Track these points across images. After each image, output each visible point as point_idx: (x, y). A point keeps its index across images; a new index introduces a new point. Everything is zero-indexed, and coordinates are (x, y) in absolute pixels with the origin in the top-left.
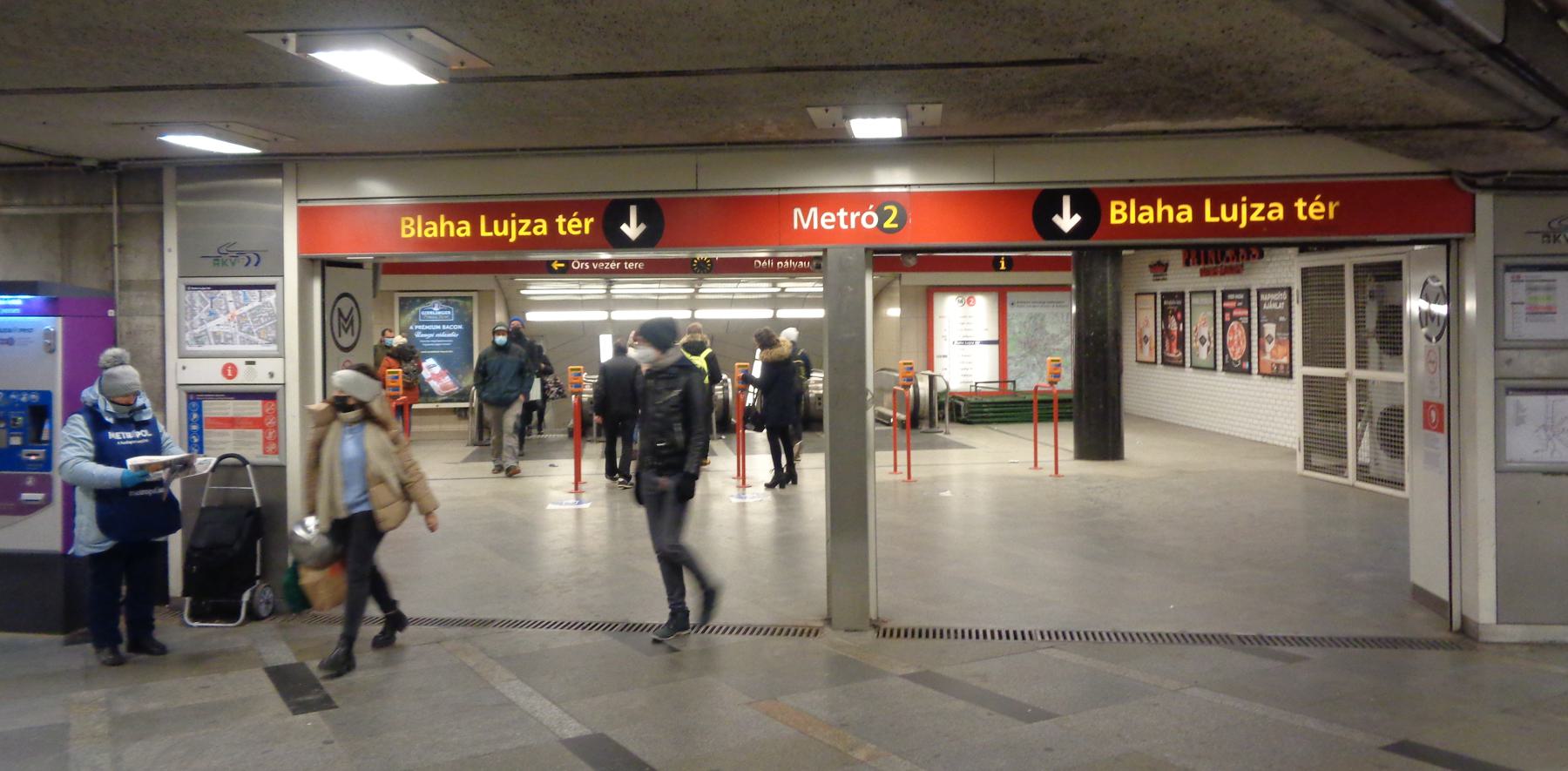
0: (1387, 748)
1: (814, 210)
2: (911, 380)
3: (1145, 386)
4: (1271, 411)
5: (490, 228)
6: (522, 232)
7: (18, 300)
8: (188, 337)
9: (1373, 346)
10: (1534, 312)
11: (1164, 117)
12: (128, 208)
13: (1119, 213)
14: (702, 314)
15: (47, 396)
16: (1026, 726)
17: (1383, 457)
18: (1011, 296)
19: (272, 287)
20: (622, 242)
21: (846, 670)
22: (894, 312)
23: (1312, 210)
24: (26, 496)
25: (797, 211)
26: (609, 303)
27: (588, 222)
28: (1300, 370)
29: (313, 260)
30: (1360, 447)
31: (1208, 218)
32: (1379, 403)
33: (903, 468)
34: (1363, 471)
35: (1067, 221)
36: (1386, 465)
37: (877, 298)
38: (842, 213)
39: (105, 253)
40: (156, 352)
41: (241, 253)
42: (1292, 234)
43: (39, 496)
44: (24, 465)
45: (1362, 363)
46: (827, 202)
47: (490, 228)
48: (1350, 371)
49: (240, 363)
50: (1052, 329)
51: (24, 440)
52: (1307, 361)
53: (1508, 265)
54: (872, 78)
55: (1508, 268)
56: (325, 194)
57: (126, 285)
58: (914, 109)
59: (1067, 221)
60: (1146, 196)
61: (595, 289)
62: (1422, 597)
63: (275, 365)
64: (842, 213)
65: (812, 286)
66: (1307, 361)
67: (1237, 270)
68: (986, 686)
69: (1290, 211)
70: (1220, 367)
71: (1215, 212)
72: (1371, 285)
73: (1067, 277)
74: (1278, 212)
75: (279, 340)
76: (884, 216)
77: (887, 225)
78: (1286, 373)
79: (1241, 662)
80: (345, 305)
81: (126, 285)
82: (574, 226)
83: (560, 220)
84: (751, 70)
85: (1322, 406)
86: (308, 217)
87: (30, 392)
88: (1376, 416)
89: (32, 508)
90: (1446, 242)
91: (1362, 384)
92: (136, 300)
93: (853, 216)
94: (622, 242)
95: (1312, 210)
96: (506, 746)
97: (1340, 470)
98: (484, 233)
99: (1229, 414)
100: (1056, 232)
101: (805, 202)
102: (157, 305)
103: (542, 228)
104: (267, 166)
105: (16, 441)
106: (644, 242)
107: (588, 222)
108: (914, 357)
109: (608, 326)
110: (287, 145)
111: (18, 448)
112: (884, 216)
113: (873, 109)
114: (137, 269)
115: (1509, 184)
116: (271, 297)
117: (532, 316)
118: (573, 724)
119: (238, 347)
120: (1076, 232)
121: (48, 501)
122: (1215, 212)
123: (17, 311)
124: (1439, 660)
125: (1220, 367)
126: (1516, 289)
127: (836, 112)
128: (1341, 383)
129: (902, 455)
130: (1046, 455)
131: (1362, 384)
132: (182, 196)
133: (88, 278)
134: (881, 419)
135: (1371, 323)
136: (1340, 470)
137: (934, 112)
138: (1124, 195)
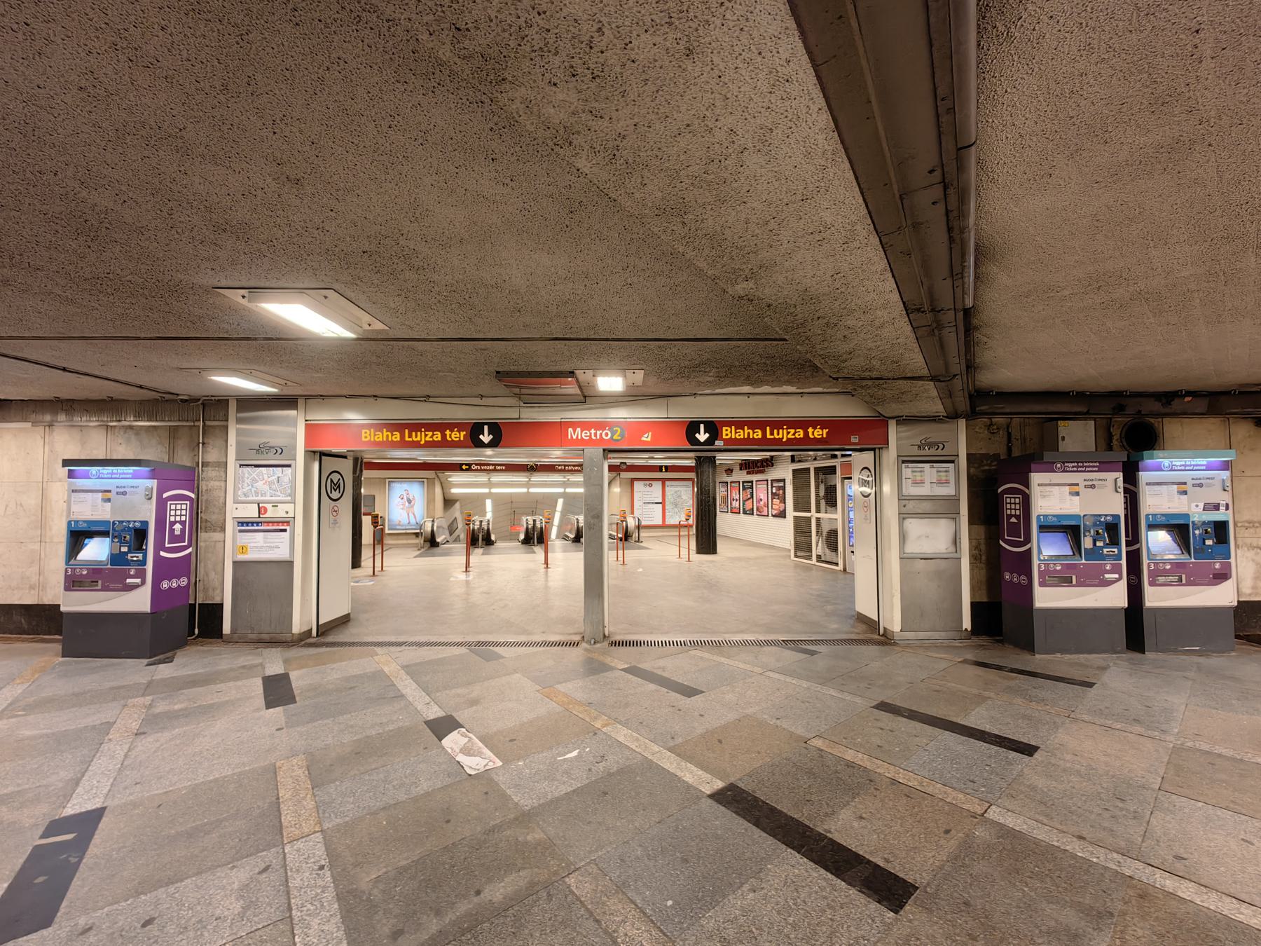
0: (877, 707)
1: (578, 430)
2: (624, 519)
3: (725, 522)
4: (782, 533)
5: (410, 436)
8: (240, 493)
9: (823, 502)
10: (915, 483)
11: (751, 384)
12: (208, 423)
13: (727, 433)
14: (532, 490)
15: (146, 523)
17: (828, 551)
18: (667, 483)
19: (289, 466)
21: (595, 668)
22: (617, 489)
23: (817, 433)
24: (129, 581)
25: (570, 430)
26: (490, 485)
27: (463, 433)
28: (791, 513)
29: (314, 452)
30: (818, 547)
31: (769, 436)
32: (826, 528)
33: (621, 559)
34: (819, 557)
35: (702, 436)
36: (829, 555)
37: (610, 483)
38: (593, 431)
39: (194, 447)
40: (222, 500)
42: (798, 447)
43: (138, 581)
44: (128, 563)
45: (818, 511)
46: (586, 426)
47: (410, 436)
48: (813, 514)
49: (269, 506)
50: (684, 497)
51: (129, 547)
52: (796, 510)
53: (904, 460)
54: (608, 344)
55: (903, 462)
56: (322, 416)
57: (205, 464)
58: (629, 373)
59: (702, 436)
60: (739, 424)
61: (482, 478)
62: (862, 619)
63: (290, 507)
64: (593, 431)
65: (579, 478)
66: (796, 510)
67: (762, 472)
68: (665, 674)
69: (806, 433)
71: (772, 433)
72: (821, 477)
73: (692, 475)
74: (800, 434)
75: (293, 494)
76: (613, 433)
78: (782, 514)
79: (789, 656)
80: (335, 477)
81: (205, 464)
82: (455, 436)
84: (541, 339)
85: (802, 528)
86: (311, 429)
88: (825, 534)
90: (874, 450)
91: (818, 520)
92: (210, 472)
94: (481, 444)
95: (817, 433)
96: (391, 727)
97: (810, 558)
99: (759, 534)
100: (697, 442)
101: (574, 425)
102: (223, 474)
103: (438, 436)
104: (286, 402)
105: (125, 549)
106: (492, 444)
107: (463, 433)
108: (626, 507)
109: (489, 495)
110: (292, 391)
111: (126, 553)
112: (613, 433)
113: (609, 369)
114: (212, 455)
115: (902, 421)
116: (288, 471)
117: (454, 491)
118: (436, 708)
119: (268, 498)
120: (708, 442)
121: (143, 583)
122: (772, 433)
124: (873, 650)
126: (907, 471)
127: (590, 373)
128: (809, 519)
129: (620, 552)
130: (684, 552)
131: (818, 520)
132: (239, 421)
133: (184, 459)
134: (611, 537)
135: (822, 493)
136: (810, 558)
137: (639, 377)
138: (729, 424)
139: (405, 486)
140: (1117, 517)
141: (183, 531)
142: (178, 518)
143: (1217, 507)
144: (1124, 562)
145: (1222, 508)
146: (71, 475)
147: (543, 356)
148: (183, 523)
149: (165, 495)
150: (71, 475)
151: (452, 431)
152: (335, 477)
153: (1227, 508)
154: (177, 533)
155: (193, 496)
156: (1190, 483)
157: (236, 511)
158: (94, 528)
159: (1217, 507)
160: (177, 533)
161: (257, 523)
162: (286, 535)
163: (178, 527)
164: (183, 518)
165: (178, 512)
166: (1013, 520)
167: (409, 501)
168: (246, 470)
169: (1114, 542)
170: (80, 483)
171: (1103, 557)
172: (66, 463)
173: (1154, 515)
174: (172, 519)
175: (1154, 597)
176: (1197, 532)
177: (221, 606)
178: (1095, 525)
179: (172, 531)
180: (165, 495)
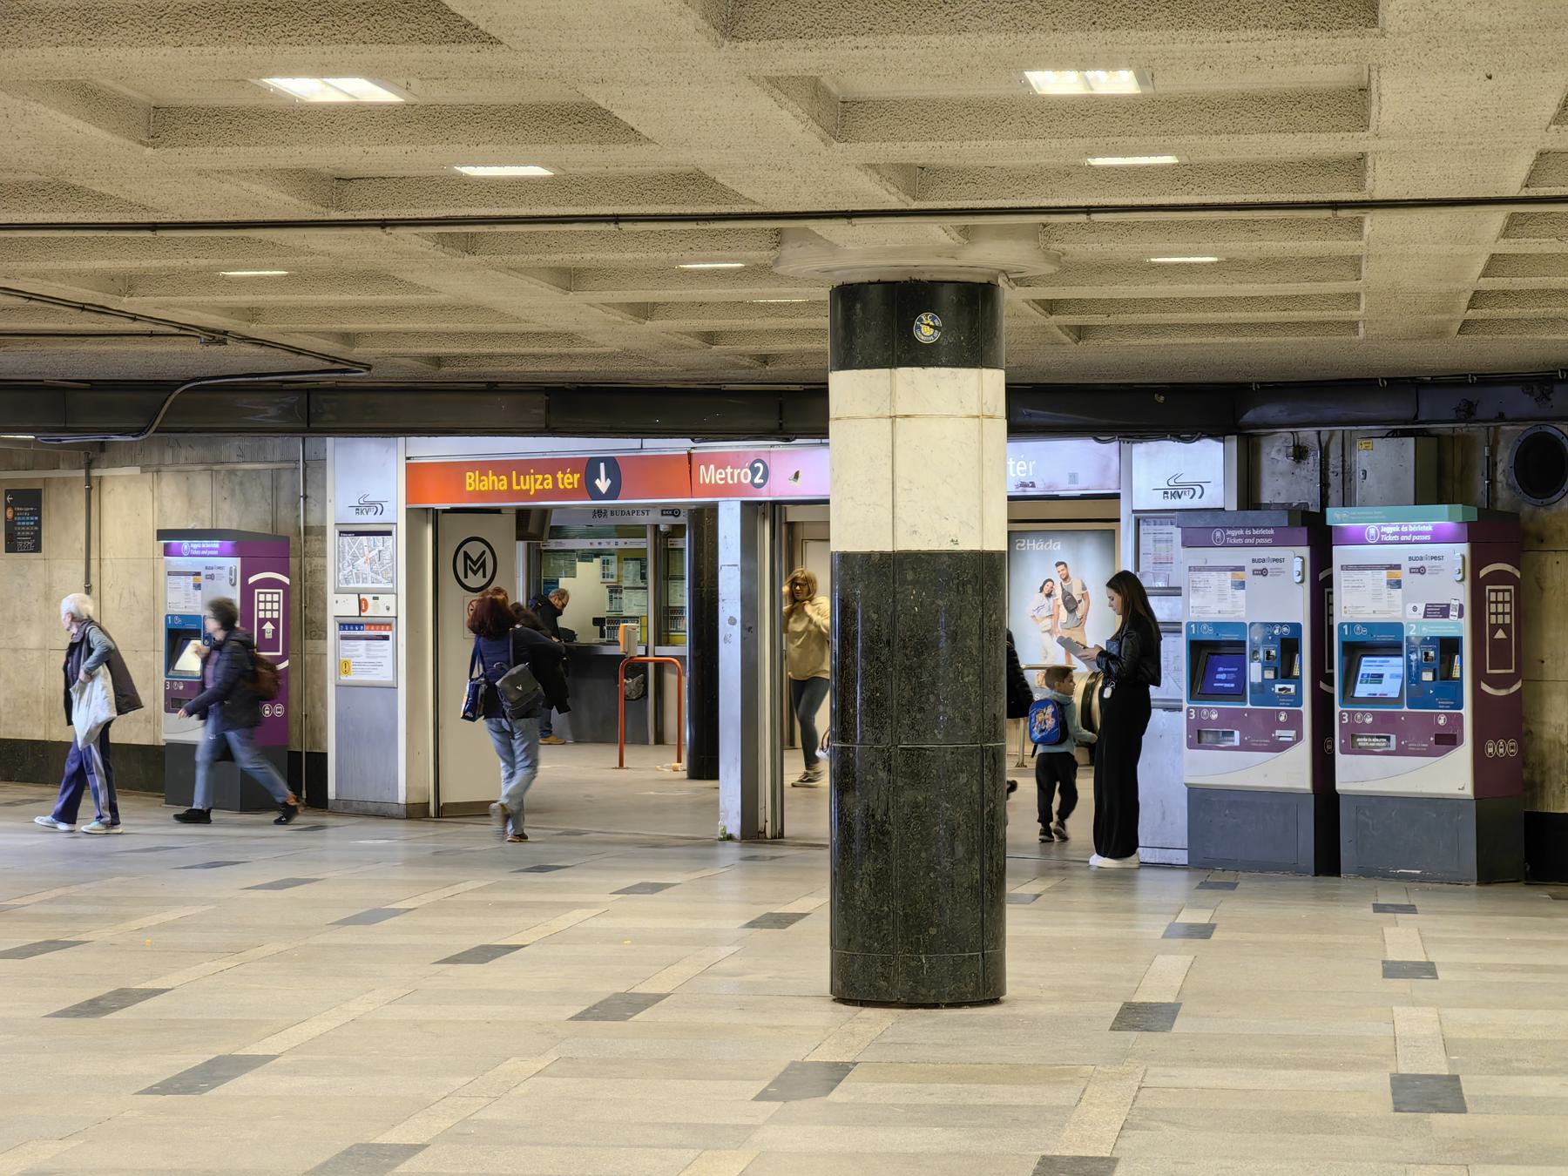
6: (538, 487)
7: (216, 544)
16: (223, 1050)
20: (595, 494)
27: (577, 476)
41: (372, 503)
43: (1293, 733)
49: (369, 598)
70: (651, 667)
77: (757, 480)
83: (560, 475)
87: (1282, 624)
89: (1280, 747)
93: (736, 472)
94: (595, 494)
98: (515, 487)
107: (577, 476)
119: (369, 585)
121: (1299, 737)
123: (1427, 537)
125: (651, 667)
139: (1057, 549)
140: (1296, 627)
141: (275, 632)
142: (269, 615)
143: (1444, 611)
144: (1306, 709)
145: (1454, 613)
146: (168, 551)
147: (95, 591)
148: (275, 622)
149: (252, 580)
150: (168, 551)
151: (564, 473)
152: (475, 550)
153: (1461, 615)
154: (268, 635)
155: (287, 581)
156: (1250, 567)
157: (340, 606)
158: (630, 849)
159: (1444, 611)
160: (268, 635)
161: (359, 626)
162: (388, 644)
163: (268, 627)
164: (276, 615)
165: (269, 605)
166: (1500, 634)
167: (1071, 604)
168: (348, 539)
169: (1286, 672)
170: (176, 562)
171: (1273, 699)
172: (162, 534)
173: (1351, 625)
174: (262, 615)
175: (1352, 774)
176: (1413, 657)
177: (325, 755)
178: (1265, 641)
179: (262, 632)
180: (252, 580)
